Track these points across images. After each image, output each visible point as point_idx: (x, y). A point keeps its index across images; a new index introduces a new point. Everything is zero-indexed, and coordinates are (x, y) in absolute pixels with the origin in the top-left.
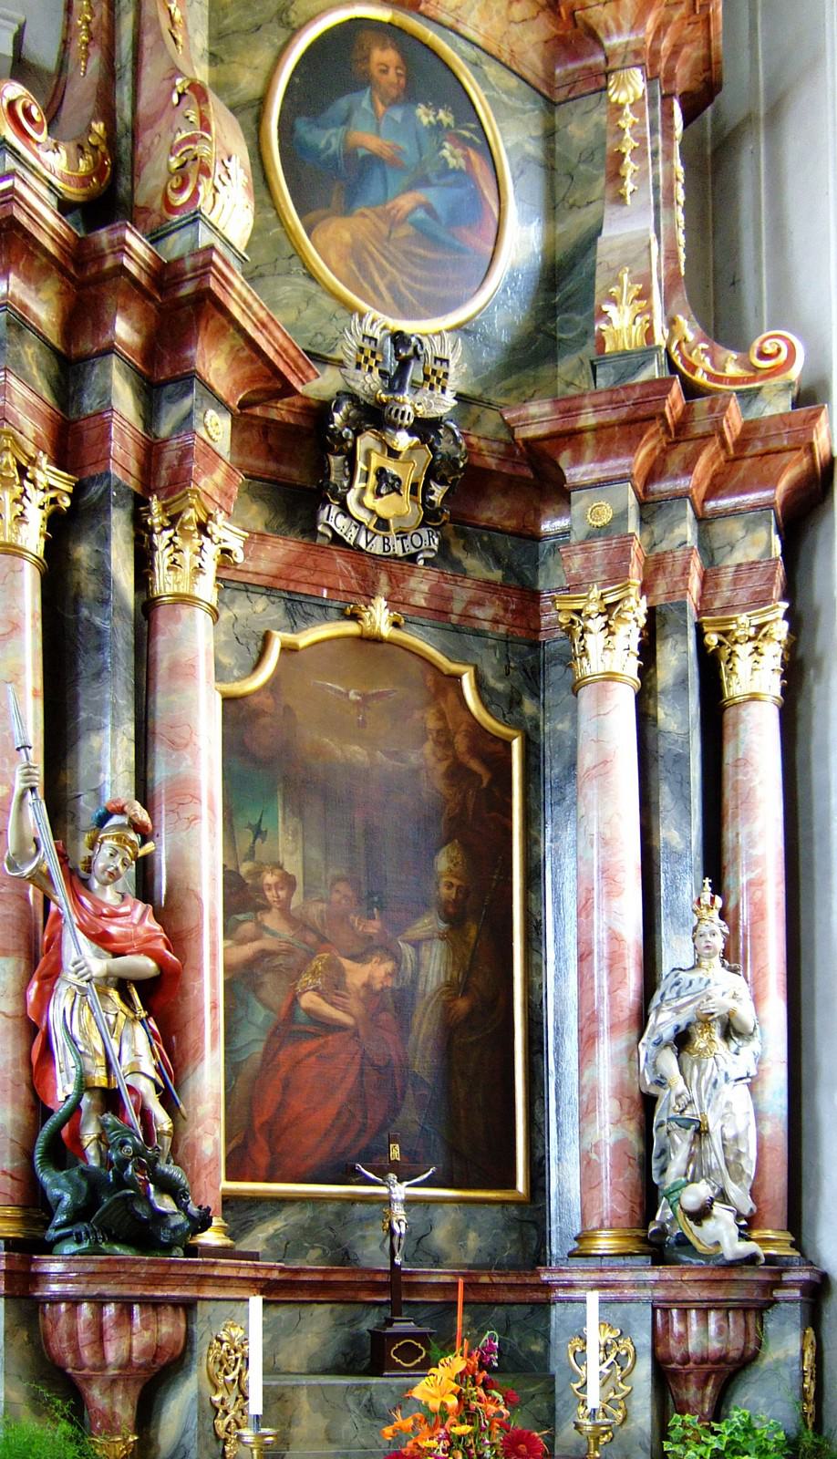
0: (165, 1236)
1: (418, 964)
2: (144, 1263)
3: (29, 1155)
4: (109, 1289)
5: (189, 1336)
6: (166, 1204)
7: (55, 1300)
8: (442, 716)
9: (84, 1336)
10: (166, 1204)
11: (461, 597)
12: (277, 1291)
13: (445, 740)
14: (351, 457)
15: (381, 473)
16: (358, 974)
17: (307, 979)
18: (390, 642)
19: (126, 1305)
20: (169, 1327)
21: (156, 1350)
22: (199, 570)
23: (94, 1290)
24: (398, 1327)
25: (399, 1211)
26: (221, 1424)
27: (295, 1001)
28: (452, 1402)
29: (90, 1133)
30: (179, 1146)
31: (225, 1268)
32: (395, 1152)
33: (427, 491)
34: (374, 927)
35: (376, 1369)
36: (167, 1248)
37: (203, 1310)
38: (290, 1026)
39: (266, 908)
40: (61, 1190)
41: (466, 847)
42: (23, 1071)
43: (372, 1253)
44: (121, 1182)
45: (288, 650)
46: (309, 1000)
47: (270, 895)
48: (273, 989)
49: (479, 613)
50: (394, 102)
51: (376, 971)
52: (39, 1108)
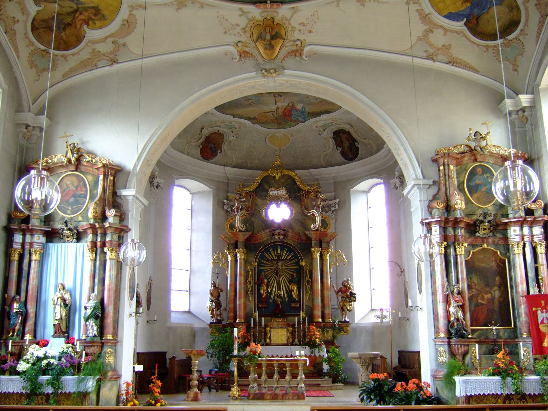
0: (465, 336)
1: (495, 294)
2: (463, 340)
3: (448, 327)
4: (459, 343)
5: (468, 350)
6: (465, 333)
7: (452, 345)
8: (495, 258)
9: (456, 349)
10: (465, 333)
11: (496, 240)
12: (479, 343)
13: (496, 261)
14: (479, 227)
15: (484, 228)
16: (486, 296)
17: (479, 298)
18: (487, 249)
19: (461, 345)
20: (466, 348)
21: (465, 351)
22: (462, 251)
23: (458, 343)
24: (495, 348)
25: (494, 331)
26: (473, 361)
27: (478, 301)
28: (502, 357)
29: (455, 324)
30: (466, 325)
31: (472, 340)
32: (493, 322)
33: (490, 229)
34: (488, 289)
35: (493, 354)
36: (465, 338)
37: (470, 345)
38: (477, 305)
39: (473, 288)
40: (453, 331)
41: (501, 276)
42: (447, 317)
43: (491, 337)
44: (460, 330)
45: (473, 252)
46: (480, 301)
47: (473, 287)
48: (474, 300)
49: (499, 242)
50: (481, 175)
51: (489, 296)
52: (449, 321)
